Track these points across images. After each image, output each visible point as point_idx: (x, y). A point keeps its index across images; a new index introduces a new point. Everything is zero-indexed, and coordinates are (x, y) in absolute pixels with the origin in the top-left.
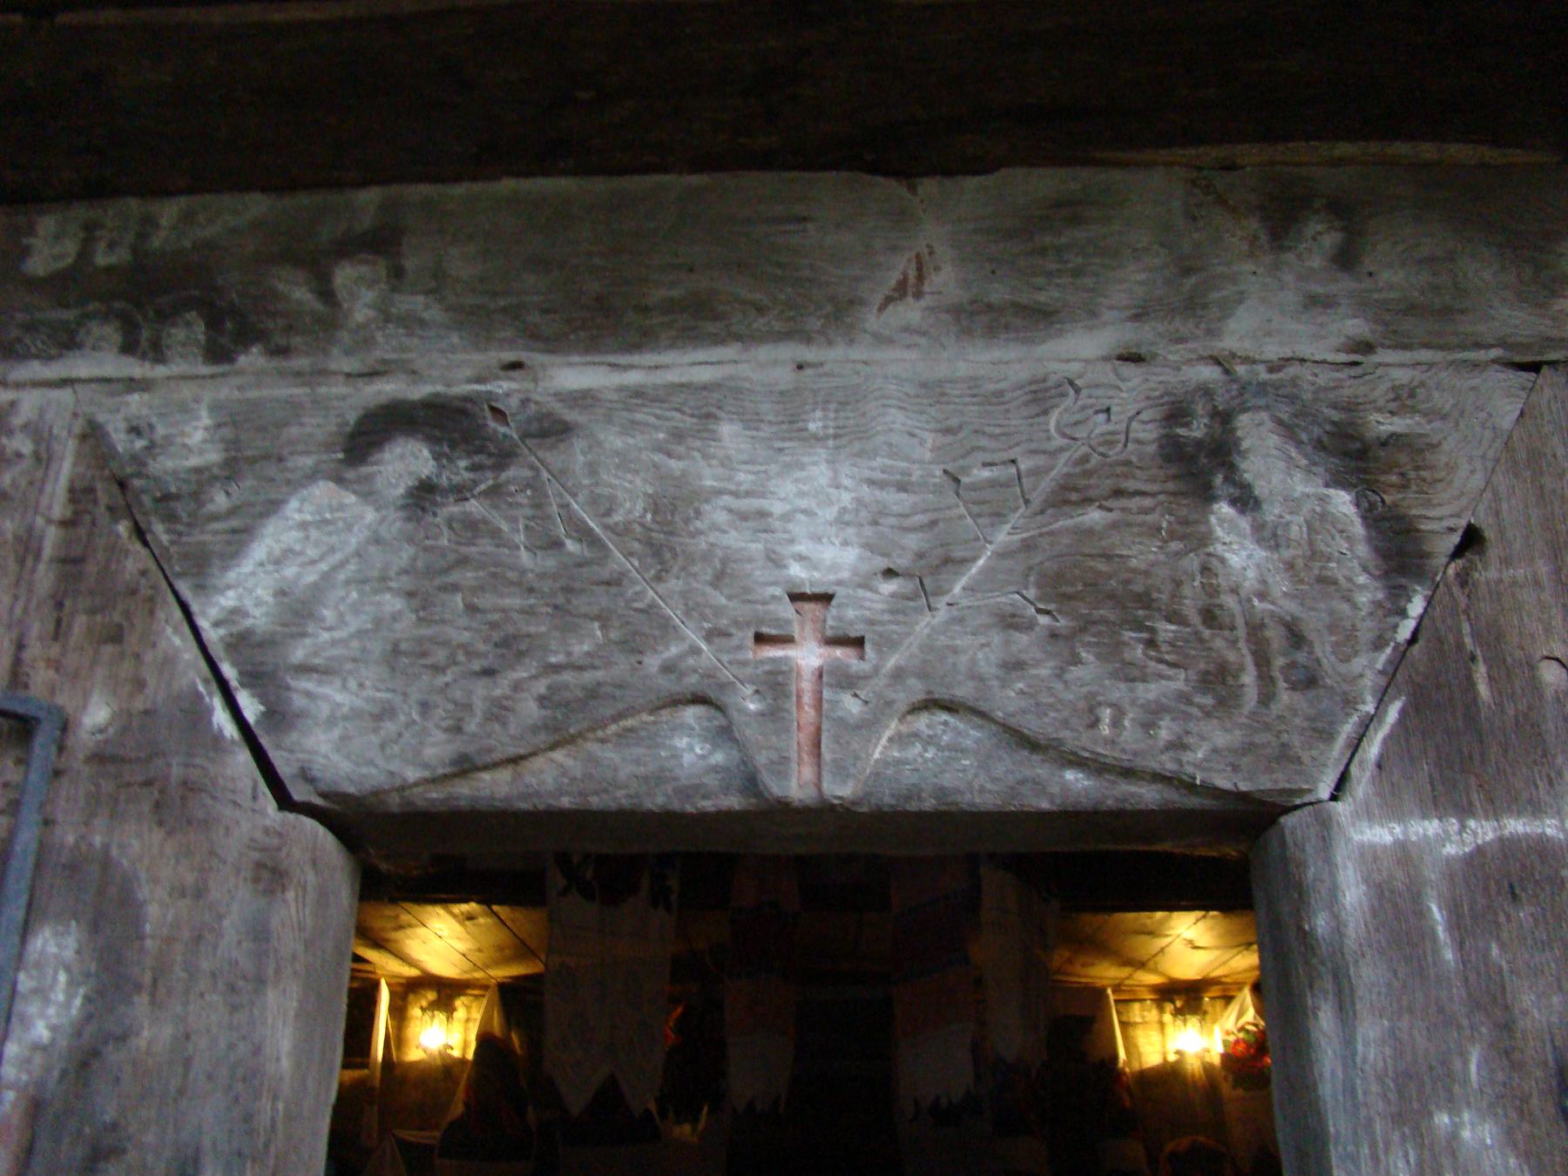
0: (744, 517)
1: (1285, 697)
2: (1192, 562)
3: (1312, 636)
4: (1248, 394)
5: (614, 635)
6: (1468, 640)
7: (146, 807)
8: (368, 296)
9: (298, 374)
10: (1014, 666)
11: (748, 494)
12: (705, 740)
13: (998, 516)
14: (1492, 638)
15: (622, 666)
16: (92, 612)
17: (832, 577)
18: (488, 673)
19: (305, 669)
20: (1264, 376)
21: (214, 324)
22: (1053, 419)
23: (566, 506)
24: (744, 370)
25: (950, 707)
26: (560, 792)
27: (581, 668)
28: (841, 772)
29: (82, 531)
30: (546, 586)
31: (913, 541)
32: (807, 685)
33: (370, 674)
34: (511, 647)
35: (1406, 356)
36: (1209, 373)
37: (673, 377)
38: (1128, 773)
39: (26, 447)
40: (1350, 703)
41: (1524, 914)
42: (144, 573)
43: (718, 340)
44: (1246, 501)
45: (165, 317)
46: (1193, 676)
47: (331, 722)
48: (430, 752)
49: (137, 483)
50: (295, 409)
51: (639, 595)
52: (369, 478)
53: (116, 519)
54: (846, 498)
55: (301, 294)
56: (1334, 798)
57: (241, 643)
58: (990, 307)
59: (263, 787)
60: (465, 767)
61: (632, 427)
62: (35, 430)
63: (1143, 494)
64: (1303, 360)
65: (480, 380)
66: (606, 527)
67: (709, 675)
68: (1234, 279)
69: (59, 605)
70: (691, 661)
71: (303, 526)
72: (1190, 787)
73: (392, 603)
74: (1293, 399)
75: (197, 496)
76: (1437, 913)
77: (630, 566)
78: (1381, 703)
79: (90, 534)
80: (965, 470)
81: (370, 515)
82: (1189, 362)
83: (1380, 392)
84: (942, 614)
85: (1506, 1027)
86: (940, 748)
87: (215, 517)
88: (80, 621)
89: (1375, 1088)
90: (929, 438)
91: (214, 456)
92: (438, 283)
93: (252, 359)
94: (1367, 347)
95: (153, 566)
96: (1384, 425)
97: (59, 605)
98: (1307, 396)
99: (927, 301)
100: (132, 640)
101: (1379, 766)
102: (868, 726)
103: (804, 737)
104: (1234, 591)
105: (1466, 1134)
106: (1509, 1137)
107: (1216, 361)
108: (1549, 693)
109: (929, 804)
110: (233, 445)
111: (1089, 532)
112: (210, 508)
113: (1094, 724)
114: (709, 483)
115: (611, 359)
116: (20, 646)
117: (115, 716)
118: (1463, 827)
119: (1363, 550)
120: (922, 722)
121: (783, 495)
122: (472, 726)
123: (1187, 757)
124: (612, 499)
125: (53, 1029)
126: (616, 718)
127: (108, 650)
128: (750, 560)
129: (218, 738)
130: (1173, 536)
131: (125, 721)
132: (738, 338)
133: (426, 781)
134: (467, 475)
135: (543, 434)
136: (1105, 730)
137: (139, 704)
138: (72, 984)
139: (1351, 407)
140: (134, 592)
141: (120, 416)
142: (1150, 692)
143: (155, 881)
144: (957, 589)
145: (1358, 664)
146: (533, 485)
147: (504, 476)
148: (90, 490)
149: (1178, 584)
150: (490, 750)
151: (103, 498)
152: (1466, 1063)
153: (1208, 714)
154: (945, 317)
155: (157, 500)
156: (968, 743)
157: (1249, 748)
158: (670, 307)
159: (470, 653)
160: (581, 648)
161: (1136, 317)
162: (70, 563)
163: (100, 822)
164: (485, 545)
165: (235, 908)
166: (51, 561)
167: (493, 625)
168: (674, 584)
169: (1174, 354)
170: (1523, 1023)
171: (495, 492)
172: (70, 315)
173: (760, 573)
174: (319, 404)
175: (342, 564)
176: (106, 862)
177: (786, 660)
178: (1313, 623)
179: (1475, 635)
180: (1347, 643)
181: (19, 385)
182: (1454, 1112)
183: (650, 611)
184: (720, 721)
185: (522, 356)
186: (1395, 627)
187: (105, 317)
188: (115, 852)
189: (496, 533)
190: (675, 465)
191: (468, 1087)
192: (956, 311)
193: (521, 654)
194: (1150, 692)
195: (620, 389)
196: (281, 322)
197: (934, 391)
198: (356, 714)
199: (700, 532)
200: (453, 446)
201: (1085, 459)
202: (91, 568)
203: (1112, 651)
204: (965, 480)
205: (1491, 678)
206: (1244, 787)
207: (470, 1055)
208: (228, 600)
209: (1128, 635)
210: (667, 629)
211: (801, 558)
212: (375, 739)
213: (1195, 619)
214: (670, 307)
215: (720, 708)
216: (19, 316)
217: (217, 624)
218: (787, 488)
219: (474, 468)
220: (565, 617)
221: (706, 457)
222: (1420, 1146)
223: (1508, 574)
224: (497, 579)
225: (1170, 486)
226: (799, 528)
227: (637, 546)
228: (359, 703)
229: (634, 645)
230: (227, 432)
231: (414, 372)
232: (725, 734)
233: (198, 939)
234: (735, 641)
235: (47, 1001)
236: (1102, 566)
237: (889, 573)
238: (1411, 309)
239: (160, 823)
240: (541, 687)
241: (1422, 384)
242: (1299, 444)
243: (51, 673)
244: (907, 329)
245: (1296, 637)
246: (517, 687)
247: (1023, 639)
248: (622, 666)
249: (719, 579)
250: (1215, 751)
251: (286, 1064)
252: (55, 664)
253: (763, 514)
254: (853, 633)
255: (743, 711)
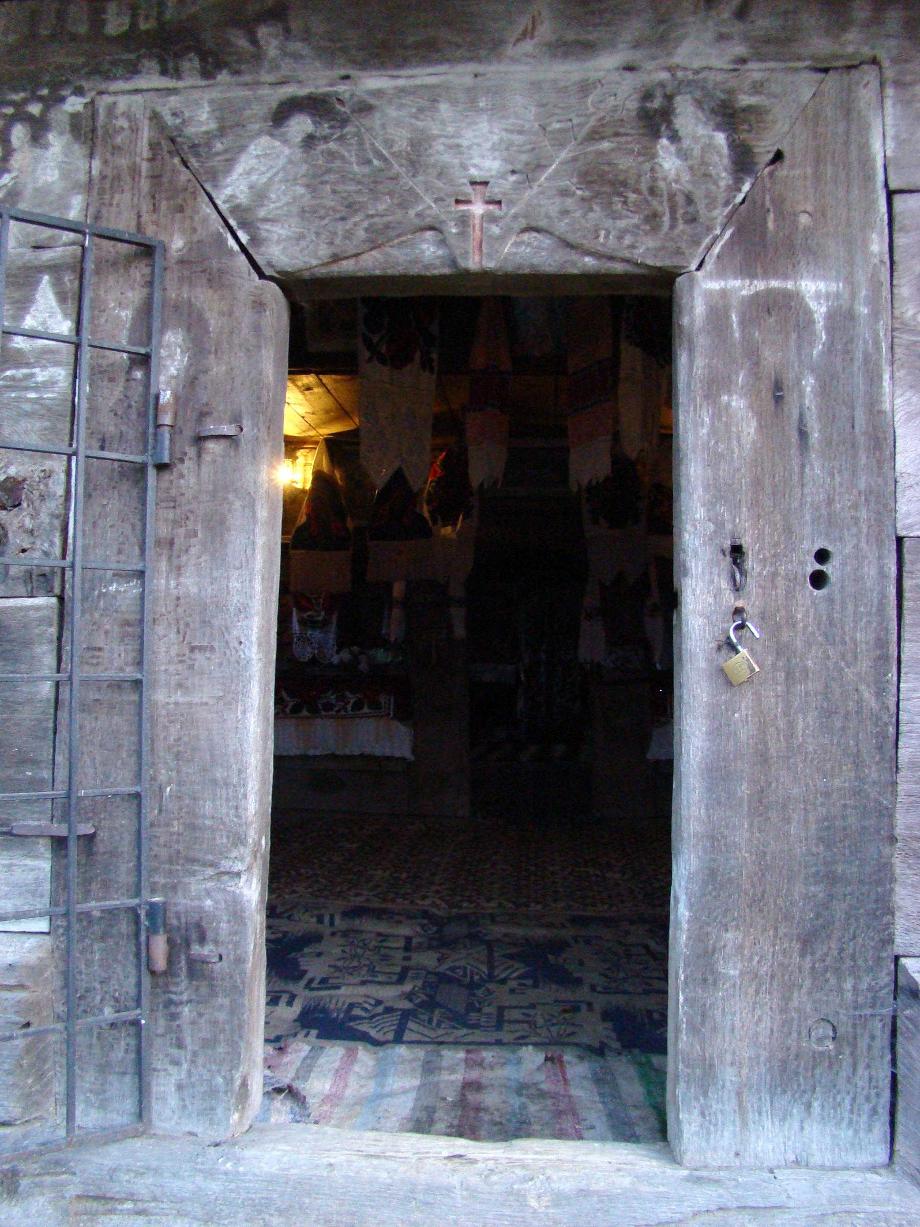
0: (450, 147)
1: (681, 226)
2: (647, 166)
3: (696, 200)
4: (682, 86)
5: (396, 201)
6: (768, 204)
7: (204, 281)
8: (275, 43)
9: (246, 84)
10: (565, 213)
11: (452, 137)
12: (434, 245)
13: (562, 145)
14: (779, 203)
15: (399, 215)
16: (168, 199)
17: (488, 174)
18: (343, 219)
19: (265, 220)
20: (691, 77)
21: (203, 59)
22: (590, 100)
23: (373, 144)
24: (451, 77)
25: (537, 230)
26: (375, 268)
27: (382, 216)
28: (490, 256)
29: (158, 163)
30: (366, 180)
31: (524, 158)
32: (477, 222)
33: (294, 221)
34: (352, 207)
35: (763, 66)
36: (664, 76)
37: (418, 82)
38: (611, 258)
39: (126, 125)
40: (709, 229)
41: (772, 320)
42: (189, 181)
43: (440, 62)
44: (675, 138)
45: (178, 56)
46: (642, 217)
47: (278, 242)
48: (321, 253)
49: (179, 139)
50: (248, 102)
51: (406, 183)
52: (284, 134)
53: (172, 157)
54: (496, 138)
55: (243, 43)
56: (698, 269)
57: (236, 210)
58: (565, 44)
59: (252, 271)
60: (336, 258)
61: (400, 107)
62: (127, 115)
63: (627, 135)
64: (711, 69)
65: (331, 85)
66: (393, 154)
67: (435, 217)
68: (683, 25)
69: (154, 197)
70: (428, 212)
71: (258, 156)
72: (636, 264)
73: (300, 190)
74: (703, 88)
75: (208, 145)
76: (734, 318)
77: (402, 170)
78: (723, 230)
79: (163, 165)
80: (550, 124)
81: (287, 151)
82: (656, 70)
83: (747, 84)
84: (536, 189)
85: (757, 364)
86: (533, 248)
87: (218, 154)
88: (164, 205)
89: (699, 385)
90: (533, 109)
91: (213, 126)
92: (306, 36)
93: (223, 77)
94: (743, 61)
95: (191, 177)
96: (745, 100)
97: (154, 197)
98: (710, 87)
99: (536, 40)
100: (188, 211)
101: (718, 257)
102: (503, 238)
103: (476, 244)
104: (665, 179)
105: (734, 404)
106: (751, 407)
107: (669, 69)
108: (801, 227)
109: (527, 271)
110: (221, 119)
111: (602, 153)
112: (214, 150)
113: (597, 237)
114: (435, 132)
115: (390, 73)
116: (139, 216)
117: (186, 244)
118: (751, 284)
119: (726, 161)
120: (526, 237)
121: (468, 137)
122: (338, 241)
123: (636, 251)
124: (393, 141)
125: (177, 370)
126: (399, 236)
127: (178, 216)
128: (454, 167)
129: (231, 251)
130: (639, 154)
131: (190, 246)
132: (448, 61)
133: (323, 265)
134: (328, 131)
135: (361, 111)
136: (601, 240)
137: (195, 238)
138: (182, 352)
139: (731, 92)
140: (186, 190)
141: (167, 107)
142: (622, 224)
143: (211, 310)
144: (542, 179)
145: (715, 213)
146: (358, 134)
147: (345, 131)
148: (159, 144)
149: (640, 176)
150: (346, 251)
151: (165, 148)
152: (738, 377)
153: (646, 234)
154: (544, 48)
155: (191, 147)
156: (545, 245)
157: (663, 248)
158: (417, 46)
159: (334, 210)
160: (382, 207)
161: (635, 47)
162: (155, 178)
163: (185, 288)
164: (338, 163)
165: (246, 319)
166: (147, 177)
167: (344, 198)
168: (421, 178)
169: (649, 65)
170: (764, 363)
171: (341, 138)
172: (132, 56)
173: (457, 173)
174: (259, 99)
175: (277, 173)
176: (190, 303)
177: (468, 210)
178: (699, 194)
179: (772, 200)
180: (712, 202)
181: (115, 93)
182: (730, 395)
183: (411, 190)
184: (441, 237)
185: (351, 72)
186: (735, 197)
187: (150, 56)
188: (193, 300)
189: (343, 158)
190: (420, 124)
191: (308, 506)
192: (549, 45)
193: (356, 211)
194: (622, 224)
195: (396, 88)
196: (235, 58)
197: (536, 86)
198: (288, 238)
199: (432, 155)
200: (320, 116)
201: (603, 118)
202: (165, 180)
203: (607, 205)
204: (548, 129)
205: (775, 220)
206: (658, 264)
207: (308, 486)
208: (228, 191)
209: (615, 199)
210: (418, 198)
211: (476, 166)
212: (297, 248)
213: (645, 192)
214: (417, 46)
215: (441, 232)
216: (108, 58)
217: (224, 202)
218: (469, 134)
219: (331, 127)
220: (375, 194)
221: (434, 120)
222: (714, 407)
223: (791, 173)
224: (344, 179)
225: (641, 131)
226: (475, 152)
227: (404, 162)
228: (289, 233)
229: (403, 205)
230: (217, 113)
231: (300, 82)
232: (443, 243)
233: (232, 332)
234: (446, 203)
235: (173, 360)
236: (606, 168)
237: (513, 172)
238: (768, 41)
239: (211, 287)
240: (366, 224)
241: (768, 80)
242: (703, 110)
243: (154, 227)
244: (526, 55)
245: (689, 200)
246: (355, 224)
247: (569, 201)
248: (399, 215)
249: (440, 175)
250: (648, 249)
251: (271, 378)
252: (156, 223)
253: (458, 146)
254: (497, 199)
255: (450, 233)
